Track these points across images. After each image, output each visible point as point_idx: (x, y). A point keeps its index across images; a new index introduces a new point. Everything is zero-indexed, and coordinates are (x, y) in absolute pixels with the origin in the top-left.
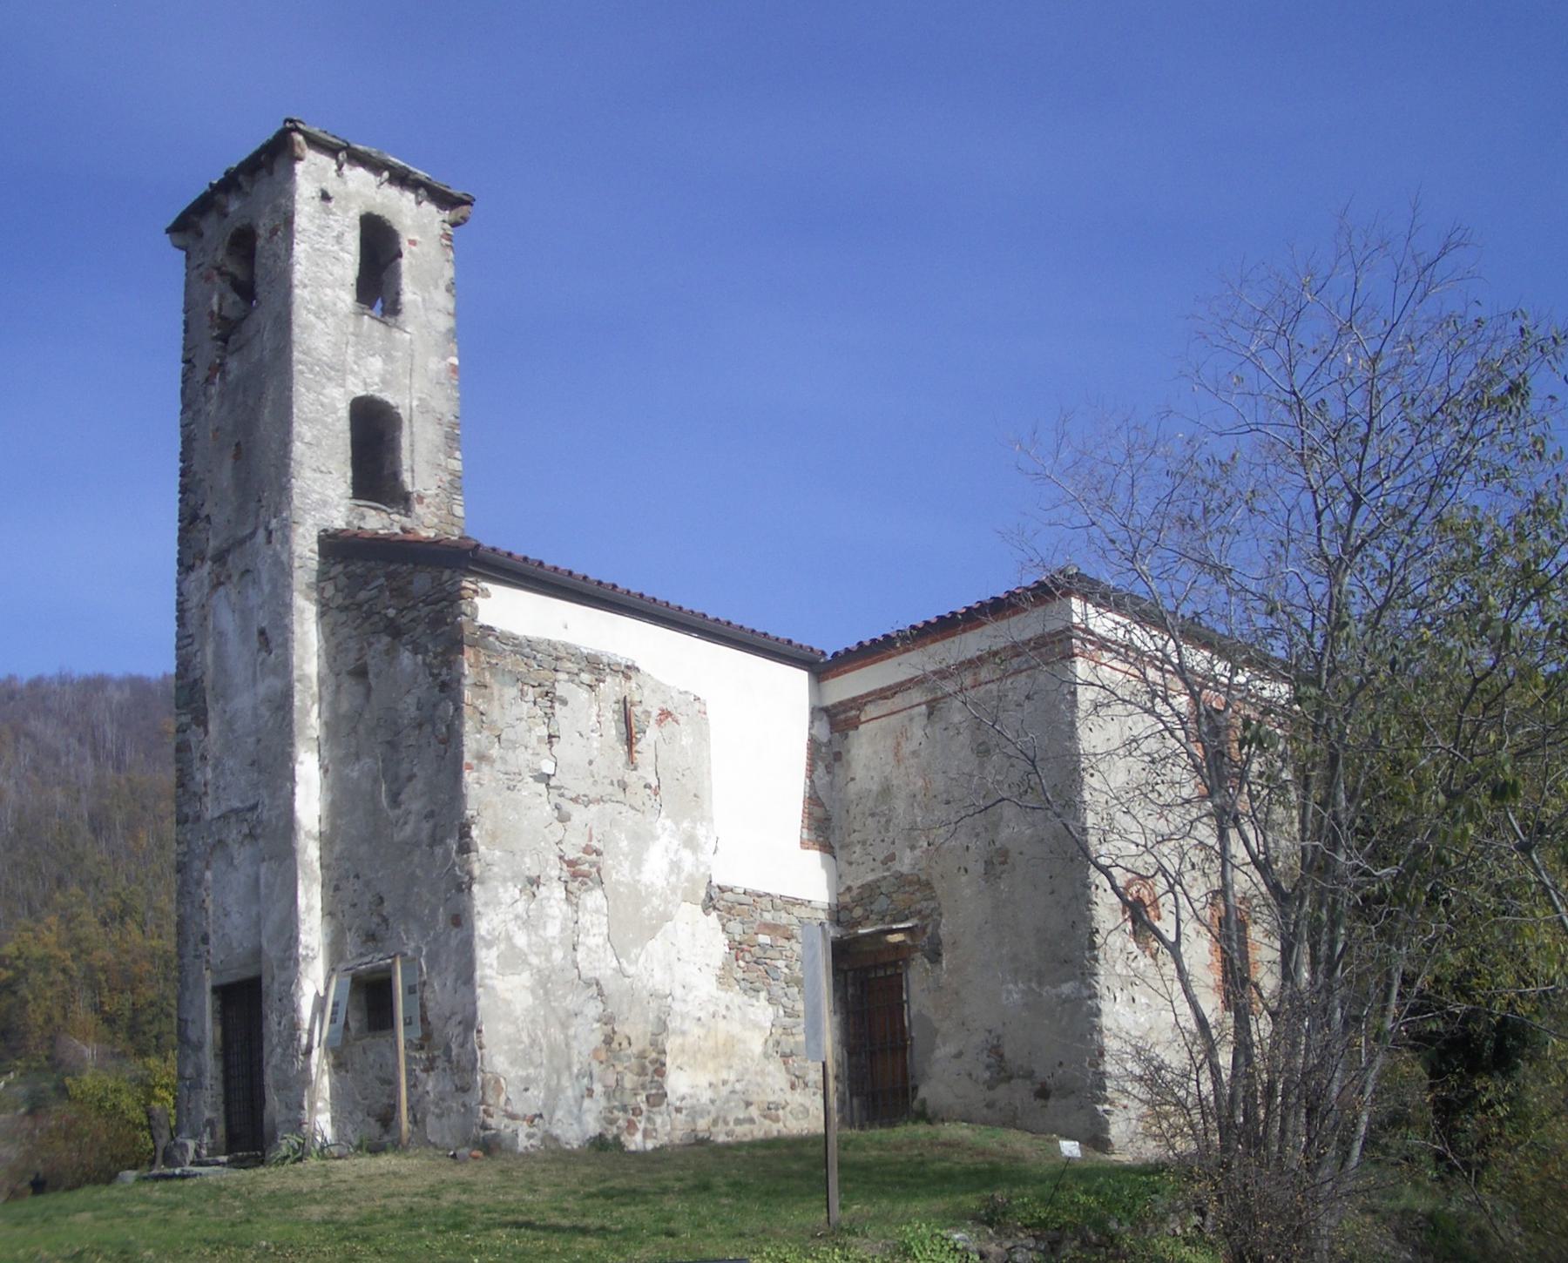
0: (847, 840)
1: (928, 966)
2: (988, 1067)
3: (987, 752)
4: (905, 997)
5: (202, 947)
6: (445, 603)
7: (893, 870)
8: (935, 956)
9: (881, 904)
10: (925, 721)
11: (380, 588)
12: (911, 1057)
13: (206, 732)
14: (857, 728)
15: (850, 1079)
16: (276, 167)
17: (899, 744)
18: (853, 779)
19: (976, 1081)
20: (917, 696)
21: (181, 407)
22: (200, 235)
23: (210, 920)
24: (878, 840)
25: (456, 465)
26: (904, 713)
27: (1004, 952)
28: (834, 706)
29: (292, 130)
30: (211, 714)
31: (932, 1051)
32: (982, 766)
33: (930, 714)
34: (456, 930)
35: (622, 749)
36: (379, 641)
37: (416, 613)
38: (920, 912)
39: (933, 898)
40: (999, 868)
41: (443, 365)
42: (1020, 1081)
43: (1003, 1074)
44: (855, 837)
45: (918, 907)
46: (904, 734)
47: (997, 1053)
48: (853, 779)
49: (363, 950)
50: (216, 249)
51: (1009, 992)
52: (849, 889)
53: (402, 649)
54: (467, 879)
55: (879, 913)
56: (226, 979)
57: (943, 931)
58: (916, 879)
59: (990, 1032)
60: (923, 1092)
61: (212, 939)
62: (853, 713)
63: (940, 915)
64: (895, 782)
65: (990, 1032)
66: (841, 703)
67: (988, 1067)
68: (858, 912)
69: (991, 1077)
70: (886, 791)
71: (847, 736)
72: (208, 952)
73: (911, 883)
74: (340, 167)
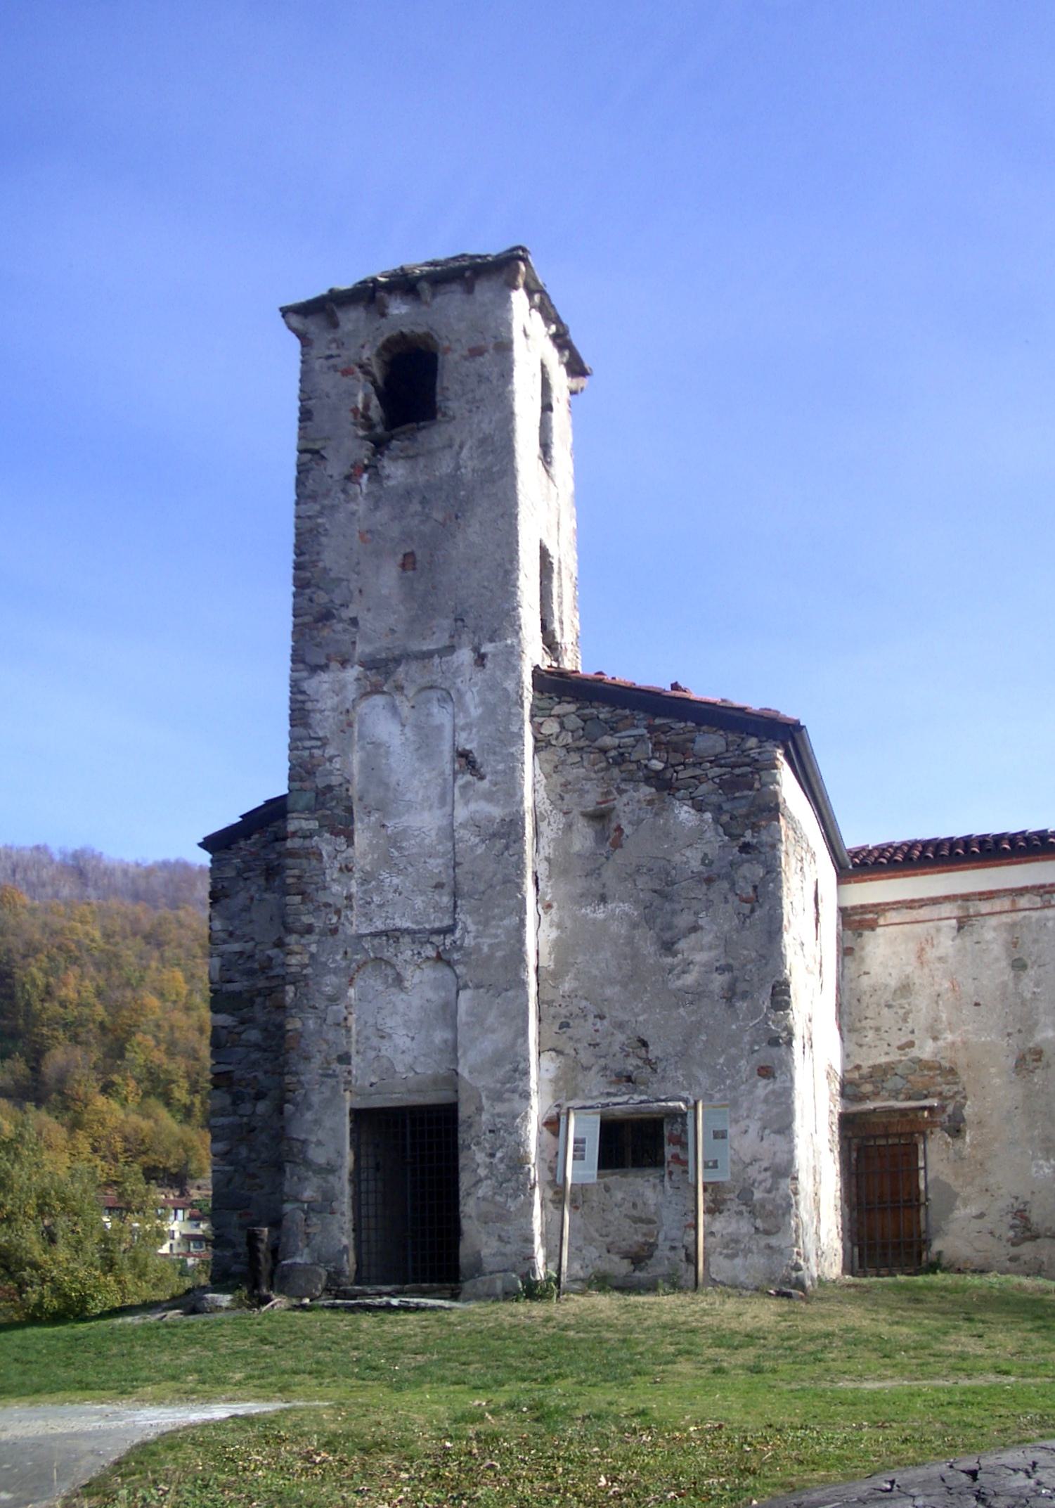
0: (858, 1025)
1: (949, 1140)
2: (1012, 1227)
3: (1024, 967)
4: (921, 1164)
5: (337, 1067)
6: (749, 769)
7: (910, 1056)
8: (956, 1131)
9: (892, 1083)
10: (955, 932)
11: (639, 739)
12: (927, 1214)
13: (350, 842)
14: (873, 929)
15: (850, 1231)
16: (477, 288)
17: (923, 949)
18: (866, 973)
19: (1000, 1238)
20: (948, 910)
21: (295, 497)
22: (335, 325)
23: (353, 1039)
24: (895, 1029)
26: (931, 924)
27: (1036, 1133)
28: (854, 908)
30: (358, 825)
31: (951, 1211)
32: (1017, 978)
33: (960, 928)
36: (636, 790)
37: (698, 772)
38: (940, 1094)
39: (956, 1083)
40: (1032, 1065)
42: (1047, 1240)
43: (1028, 1234)
44: (869, 1023)
45: (939, 1089)
46: (930, 941)
47: (1022, 1217)
48: (866, 973)
49: (612, 1090)
50: (363, 347)
51: (1041, 1167)
52: (858, 1067)
53: (678, 803)
54: (784, 1034)
55: (891, 1091)
56: (362, 1104)
57: (967, 1112)
58: (937, 1065)
59: (1017, 1198)
60: (937, 1245)
61: (355, 1060)
62: (870, 916)
63: (965, 1098)
64: (917, 981)
65: (1017, 1198)
66: (862, 907)
67: (1012, 1227)
68: (867, 1088)
69: (1016, 1236)
70: (905, 989)
71: (860, 935)
72: (350, 1072)
73: (930, 1069)
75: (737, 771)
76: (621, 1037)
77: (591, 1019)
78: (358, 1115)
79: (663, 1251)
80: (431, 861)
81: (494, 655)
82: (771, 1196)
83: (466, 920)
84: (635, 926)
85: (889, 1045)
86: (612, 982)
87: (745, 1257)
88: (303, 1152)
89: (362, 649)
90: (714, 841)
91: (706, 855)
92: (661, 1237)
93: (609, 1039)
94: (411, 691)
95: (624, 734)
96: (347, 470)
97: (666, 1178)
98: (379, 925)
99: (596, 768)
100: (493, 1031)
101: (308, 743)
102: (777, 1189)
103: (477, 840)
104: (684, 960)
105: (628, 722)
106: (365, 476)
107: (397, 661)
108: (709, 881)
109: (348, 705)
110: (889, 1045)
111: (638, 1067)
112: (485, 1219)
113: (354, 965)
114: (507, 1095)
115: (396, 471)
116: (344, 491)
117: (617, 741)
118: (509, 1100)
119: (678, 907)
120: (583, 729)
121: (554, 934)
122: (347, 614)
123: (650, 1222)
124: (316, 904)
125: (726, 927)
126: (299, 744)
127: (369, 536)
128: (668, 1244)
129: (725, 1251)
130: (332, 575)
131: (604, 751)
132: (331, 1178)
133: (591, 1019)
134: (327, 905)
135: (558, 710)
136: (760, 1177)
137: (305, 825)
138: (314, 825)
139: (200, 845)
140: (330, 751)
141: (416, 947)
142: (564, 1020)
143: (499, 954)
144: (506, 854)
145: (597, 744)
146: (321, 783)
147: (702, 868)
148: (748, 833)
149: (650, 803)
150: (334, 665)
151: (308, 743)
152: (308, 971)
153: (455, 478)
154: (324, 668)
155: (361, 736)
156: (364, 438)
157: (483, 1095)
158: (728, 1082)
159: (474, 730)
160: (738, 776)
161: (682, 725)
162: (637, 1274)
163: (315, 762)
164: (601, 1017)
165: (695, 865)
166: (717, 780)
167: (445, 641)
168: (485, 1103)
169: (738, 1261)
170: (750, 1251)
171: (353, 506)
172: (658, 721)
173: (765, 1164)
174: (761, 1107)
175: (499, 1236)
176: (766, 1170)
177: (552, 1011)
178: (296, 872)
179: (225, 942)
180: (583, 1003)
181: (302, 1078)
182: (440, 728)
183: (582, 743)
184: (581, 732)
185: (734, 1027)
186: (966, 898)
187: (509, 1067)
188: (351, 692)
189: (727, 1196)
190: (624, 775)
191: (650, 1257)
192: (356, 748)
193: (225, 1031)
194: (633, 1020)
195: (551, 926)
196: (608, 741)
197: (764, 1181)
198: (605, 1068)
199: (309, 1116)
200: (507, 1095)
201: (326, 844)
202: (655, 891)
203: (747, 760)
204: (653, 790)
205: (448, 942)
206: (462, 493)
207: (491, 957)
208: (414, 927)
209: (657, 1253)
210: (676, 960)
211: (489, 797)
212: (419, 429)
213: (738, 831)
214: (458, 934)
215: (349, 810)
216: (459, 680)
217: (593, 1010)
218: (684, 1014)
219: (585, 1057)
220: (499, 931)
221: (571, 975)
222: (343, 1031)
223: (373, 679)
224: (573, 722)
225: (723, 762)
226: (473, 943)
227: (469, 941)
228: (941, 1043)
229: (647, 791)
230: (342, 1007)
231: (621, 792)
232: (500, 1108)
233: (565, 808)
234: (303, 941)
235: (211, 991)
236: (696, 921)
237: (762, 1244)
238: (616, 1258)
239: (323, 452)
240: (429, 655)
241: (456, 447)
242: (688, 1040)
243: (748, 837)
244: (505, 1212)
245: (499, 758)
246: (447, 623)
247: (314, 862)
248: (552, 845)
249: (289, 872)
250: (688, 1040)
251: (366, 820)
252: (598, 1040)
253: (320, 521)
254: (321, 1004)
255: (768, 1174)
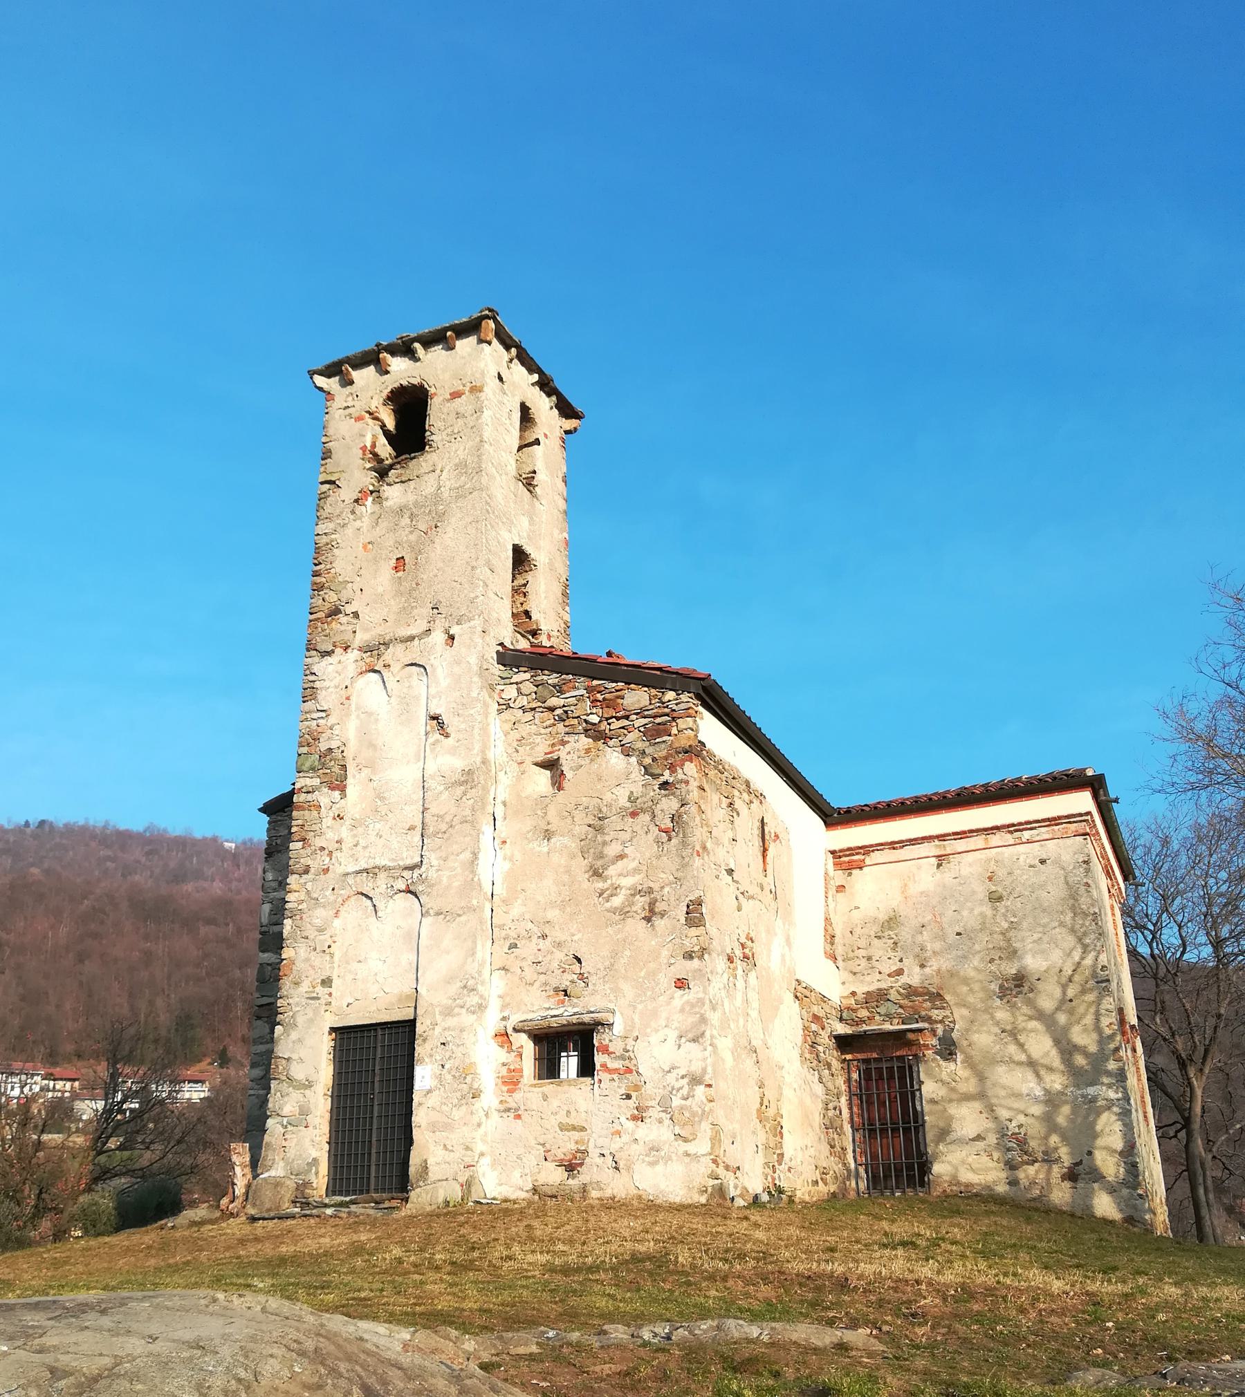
5: (321, 990)
11: (580, 698)
23: (336, 965)
25: (567, 617)
29: (487, 317)
30: (350, 781)
33: (939, 866)
34: (680, 992)
35: (761, 858)
39: (943, 1008)
41: (560, 536)
68: (864, 1013)
72: (330, 994)
74: (511, 361)
75: (658, 720)
76: (559, 955)
77: (534, 939)
78: (341, 1033)
79: (593, 1158)
80: (406, 808)
81: (460, 635)
82: (688, 1103)
83: (432, 858)
84: (573, 857)
85: (880, 973)
86: (552, 904)
87: (666, 1164)
88: (287, 1069)
89: (361, 638)
90: (636, 782)
91: (632, 792)
92: (591, 1145)
93: (549, 957)
94: (396, 667)
95: (567, 695)
96: (355, 495)
97: (596, 1085)
98: (363, 864)
99: (545, 725)
100: (448, 952)
101: (315, 715)
102: (693, 1096)
103: (442, 788)
104: (612, 884)
105: (571, 685)
106: (370, 499)
107: (386, 645)
108: (634, 814)
109: (348, 683)
110: (880, 973)
111: (572, 982)
112: (434, 1127)
113: (340, 900)
114: (457, 1010)
115: (394, 494)
116: (353, 512)
117: (562, 702)
118: (459, 1014)
119: (608, 838)
120: (536, 693)
121: (507, 865)
122: (349, 609)
123: (583, 1129)
124: (313, 848)
125: (648, 855)
126: (308, 716)
127: (370, 546)
128: (599, 1151)
129: (647, 1159)
130: (340, 579)
131: (552, 709)
132: (307, 1092)
133: (534, 939)
134: (323, 849)
135: (516, 678)
136: (677, 1085)
137: (308, 782)
138: (317, 781)
139: (260, 810)
140: (332, 720)
141: (391, 882)
142: (512, 941)
143: (456, 884)
144: (464, 798)
145: (546, 705)
146: (323, 746)
147: (628, 805)
148: (667, 773)
149: (588, 751)
150: (339, 651)
151: (315, 715)
152: (303, 906)
153: (437, 497)
154: (329, 653)
155: (358, 708)
156: (370, 469)
157: (437, 1010)
158: (649, 993)
159: (443, 697)
160: (659, 724)
161: (614, 685)
162: (571, 1182)
163: (320, 730)
164: (544, 937)
165: (623, 802)
166: (642, 729)
167: (425, 626)
168: (439, 1018)
169: (659, 1168)
170: (670, 1159)
171: (358, 524)
172: (595, 682)
173: (683, 1072)
174: (677, 1017)
175: (445, 1145)
176: (683, 1077)
177: (503, 933)
178: (300, 822)
179: (275, 890)
180: (530, 925)
181: (291, 1001)
182: (417, 698)
183: (534, 705)
184: (534, 696)
185: (653, 943)
186: (942, 837)
187: (459, 984)
188: (352, 669)
189: (650, 1103)
190: (567, 729)
191: (581, 1164)
192: (353, 717)
193: (269, 968)
194: (569, 939)
195: (505, 859)
196: (553, 701)
197: (681, 1088)
198: (546, 984)
199: (294, 1035)
200: (457, 1010)
201: (325, 797)
202: (589, 826)
203: (667, 710)
204: (591, 740)
205: (415, 875)
206: (441, 507)
207: (448, 887)
208: (391, 864)
209: (587, 1160)
210: (606, 885)
211: (453, 751)
212: (412, 459)
213: (658, 771)
214: (423, 869)
215: (344, 767)
216: (432, 657)
217: (536, 931)
218: (611, 932)
219: (529, 973)
220: (456, 865)
221: (519, 901)
222: (328, 958)
223: (368, 660)
224: (528, 687)
225: (646, 713)
226: (435, 876)
227: (432, 874)
228: (927, 970)
229: (585, 741)
230: (327, 936)
231: (563, 743)
232: (451, 1022)
233: (519, 760)
234: (302, 881)
235: (261, 933)
236: (623, 850)
237: (681, 1151)
238: (551, 1166)
239: (337, 482)
240: (411, 638)
241: (438, 471)
242: (615, 955)
243: (667, 776)
244: (450, 1121)
245: (461, 719)
246: (426, 611)
247: (315, 813)
248: (507, 790)
249: (294, 823)
250: (615, 955)
251: (358, 776)
252: (540, 959)
253: (333, 536)
254: (311, 933)
255: (686, 1080)
